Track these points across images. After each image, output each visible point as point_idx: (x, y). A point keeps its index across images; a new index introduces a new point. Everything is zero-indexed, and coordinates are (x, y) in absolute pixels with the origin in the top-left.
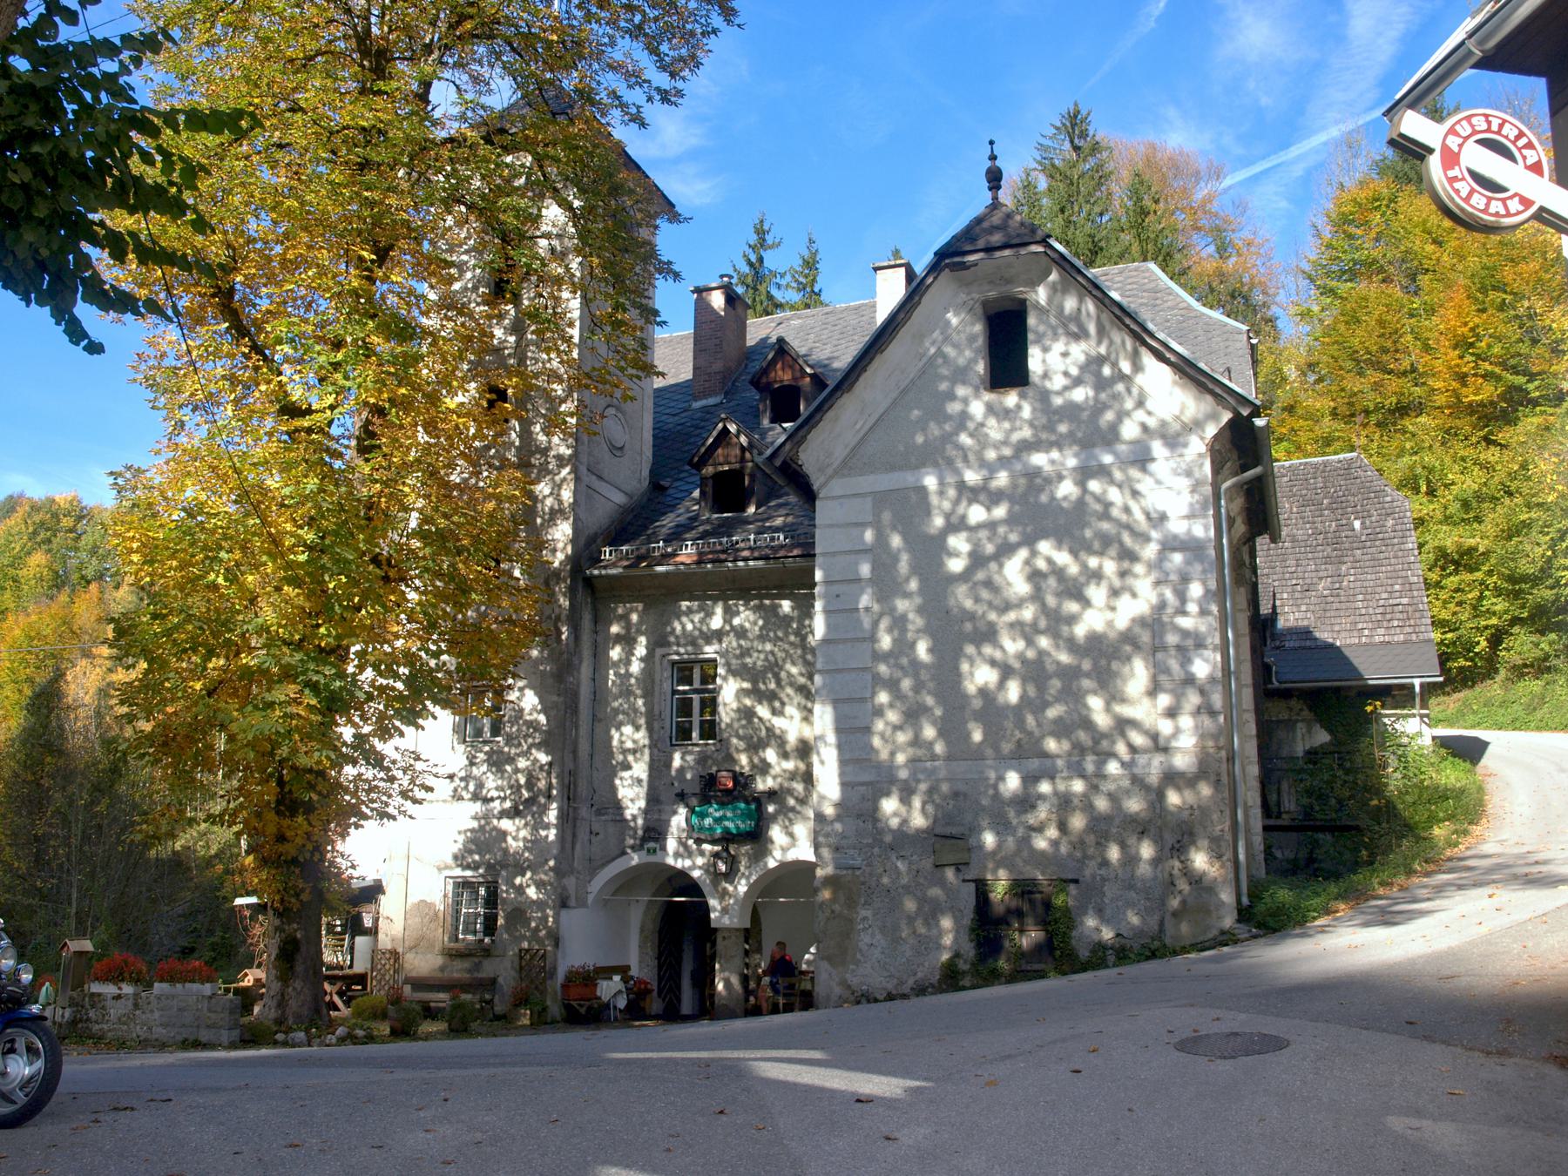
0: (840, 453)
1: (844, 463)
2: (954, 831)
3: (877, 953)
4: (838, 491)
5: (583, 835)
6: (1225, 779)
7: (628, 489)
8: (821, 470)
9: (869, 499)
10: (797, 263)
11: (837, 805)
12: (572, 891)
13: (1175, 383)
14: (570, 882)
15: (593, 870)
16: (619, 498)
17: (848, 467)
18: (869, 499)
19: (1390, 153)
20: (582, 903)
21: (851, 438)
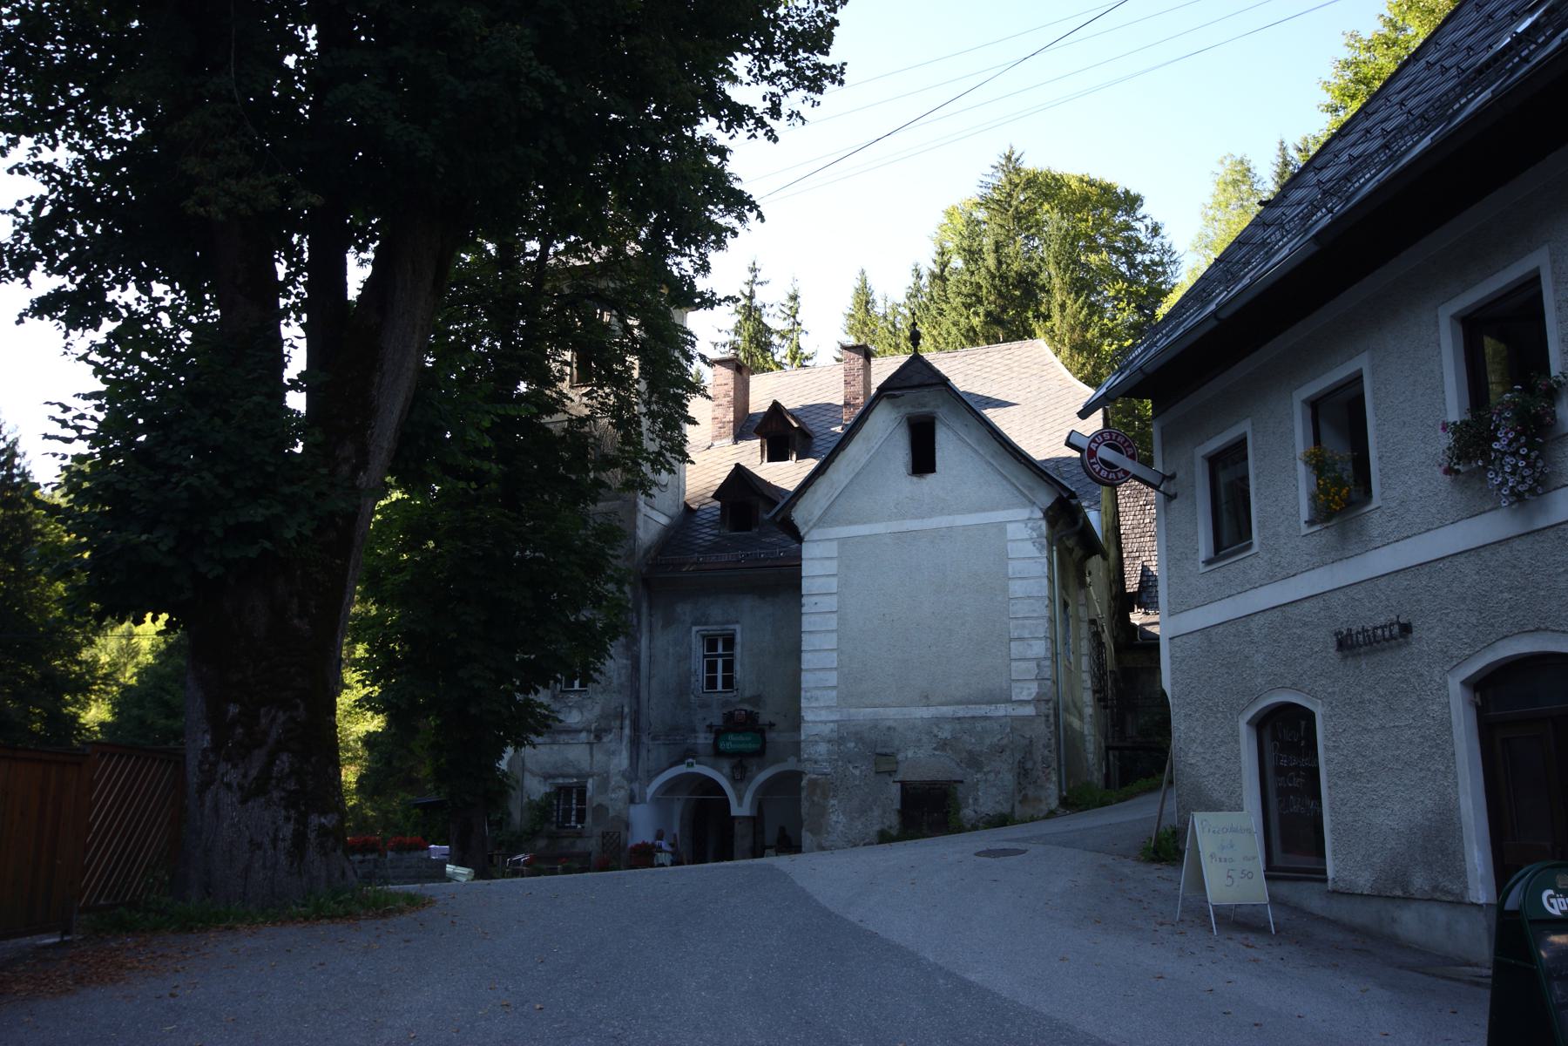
0: (817, 513)
1: (820, 519)
2: (887, 751)
3: (840, 827)
4: (816, 537)
5: (644, 753)
6: (1052, 719)
7: (670, 513)
8: (806, 523)
9: (835, 543)
10: (784, 299)
11: (144, 672)
12: (637, 791)
13: (1293, 140)
14: (636, 786)
15: (650, 779)
16: (664, 520)
17: (822, 521)
18: (835, 543)
19: (1260, 208)
20: (643, 801)
21: (824, 503)
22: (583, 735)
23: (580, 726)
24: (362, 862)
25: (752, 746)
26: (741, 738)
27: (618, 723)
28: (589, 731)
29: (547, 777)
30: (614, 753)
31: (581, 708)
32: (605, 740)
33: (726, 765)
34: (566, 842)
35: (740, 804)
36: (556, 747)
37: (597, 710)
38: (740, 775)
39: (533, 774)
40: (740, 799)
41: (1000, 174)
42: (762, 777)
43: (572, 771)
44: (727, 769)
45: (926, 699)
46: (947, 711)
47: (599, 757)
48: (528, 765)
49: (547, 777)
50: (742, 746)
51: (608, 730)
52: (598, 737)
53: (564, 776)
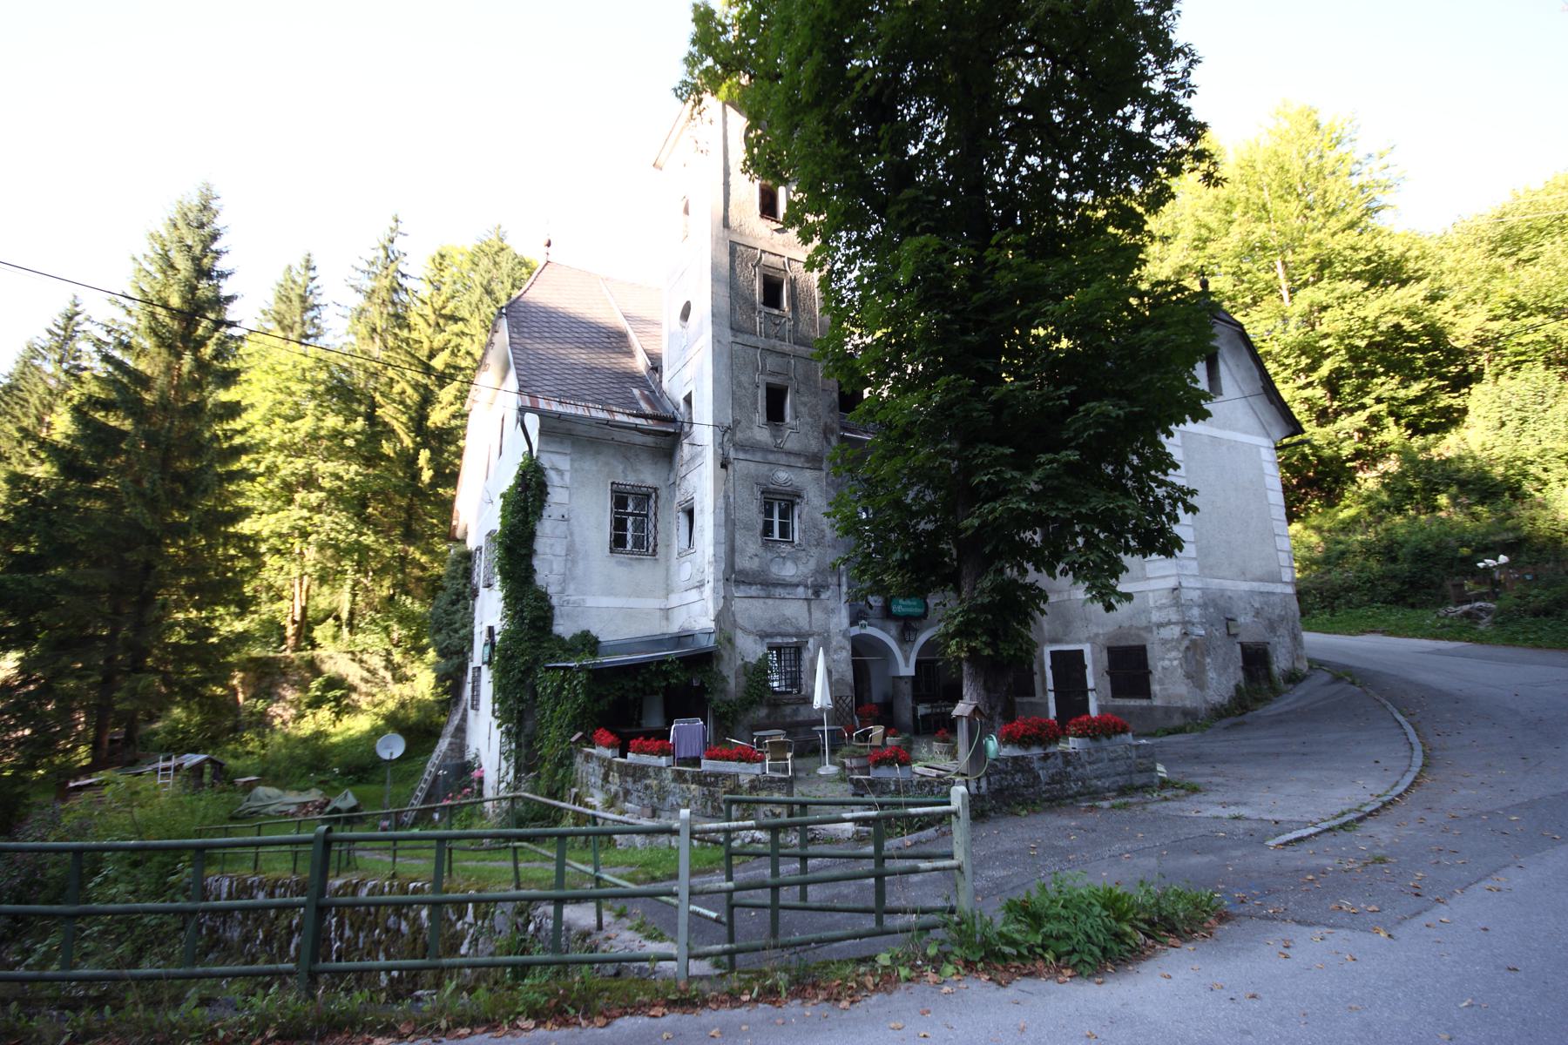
22: (801, 589)
23: (795, 580)
24: (1046, 757)
25: (919, 611)
26: (908, 602)
27: (835, 580)
28: (806, 586)
29: (763, 636)
30: (833, 611)
31: (795, 561)
32: (823, 596)
33: (893, 628)
34: (788, 710)
35: (907, 664)
36: (770, 602)
37: (812, 564)
38: (905, 638)
39: (744, 630)
40: (907, 660)
41: (136, 307)
42: (922, 638)
43: (791, 630)
44: (894, 632)
45: (1243, 575)
46: (1256, 586)
47: (818, 614)
48: (740, 621)
49: (763, 636)
50: (910, 610)
51: (827, 587)
52: (817, 594)
53: (783, 635)
